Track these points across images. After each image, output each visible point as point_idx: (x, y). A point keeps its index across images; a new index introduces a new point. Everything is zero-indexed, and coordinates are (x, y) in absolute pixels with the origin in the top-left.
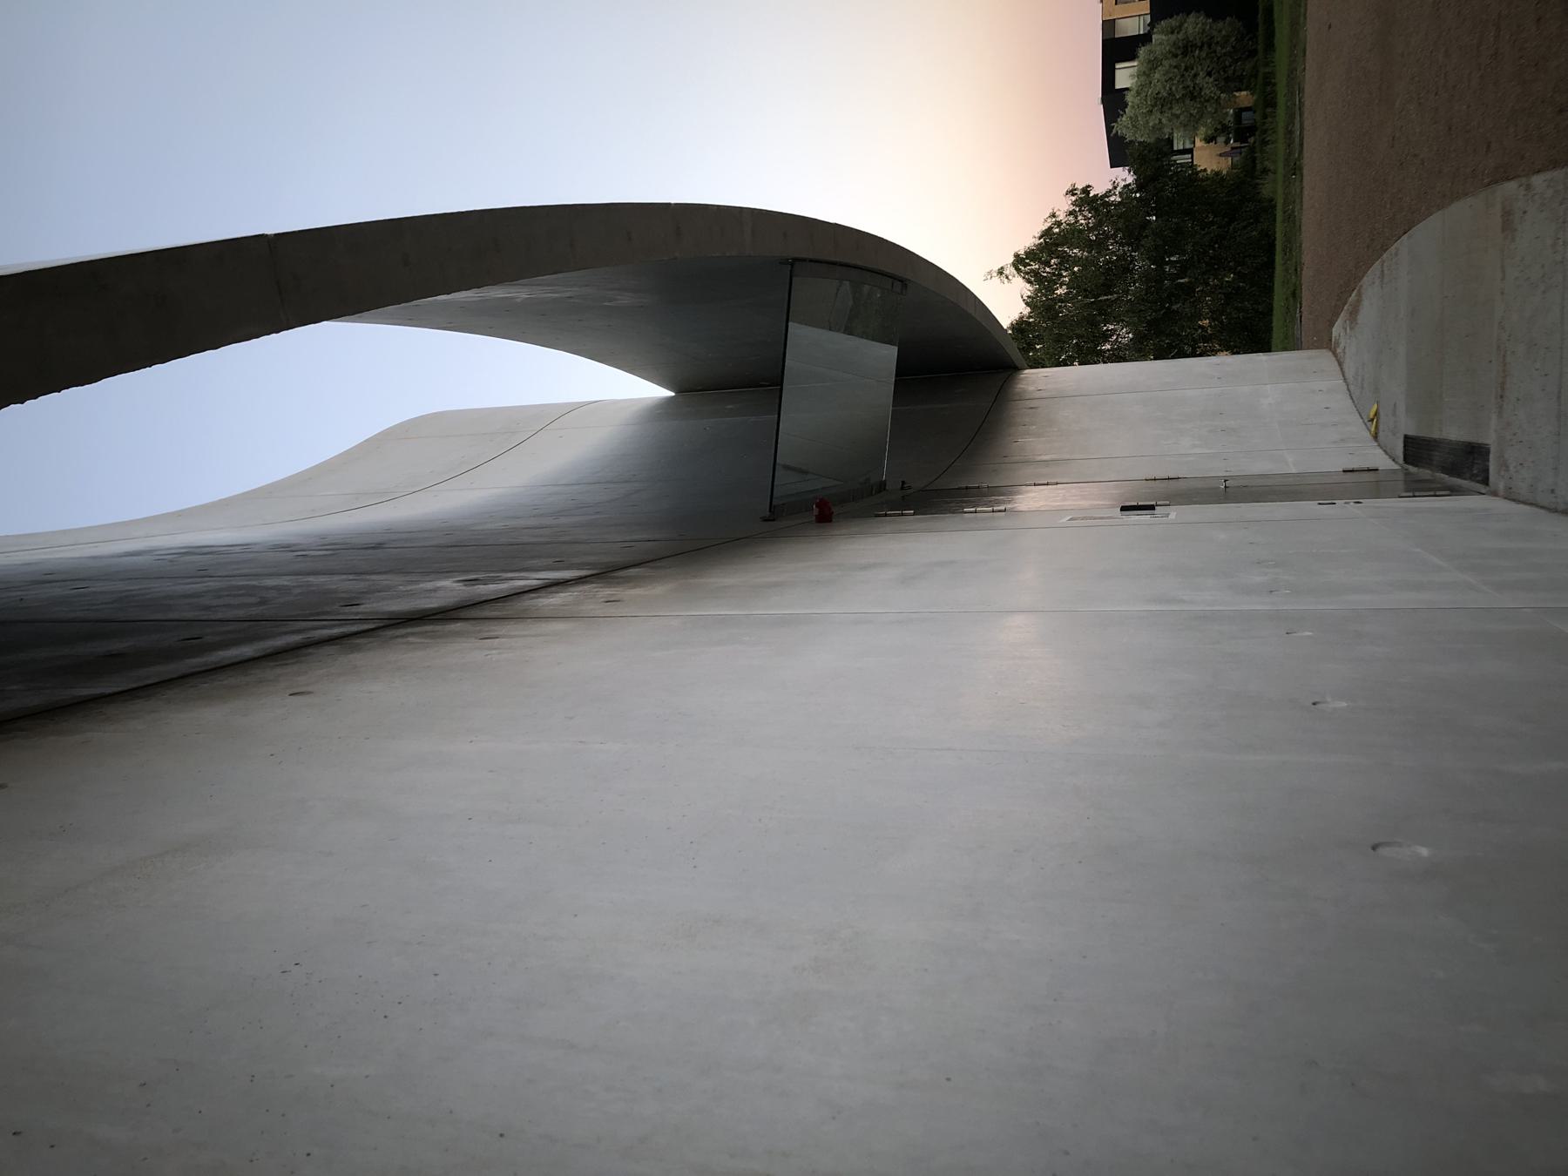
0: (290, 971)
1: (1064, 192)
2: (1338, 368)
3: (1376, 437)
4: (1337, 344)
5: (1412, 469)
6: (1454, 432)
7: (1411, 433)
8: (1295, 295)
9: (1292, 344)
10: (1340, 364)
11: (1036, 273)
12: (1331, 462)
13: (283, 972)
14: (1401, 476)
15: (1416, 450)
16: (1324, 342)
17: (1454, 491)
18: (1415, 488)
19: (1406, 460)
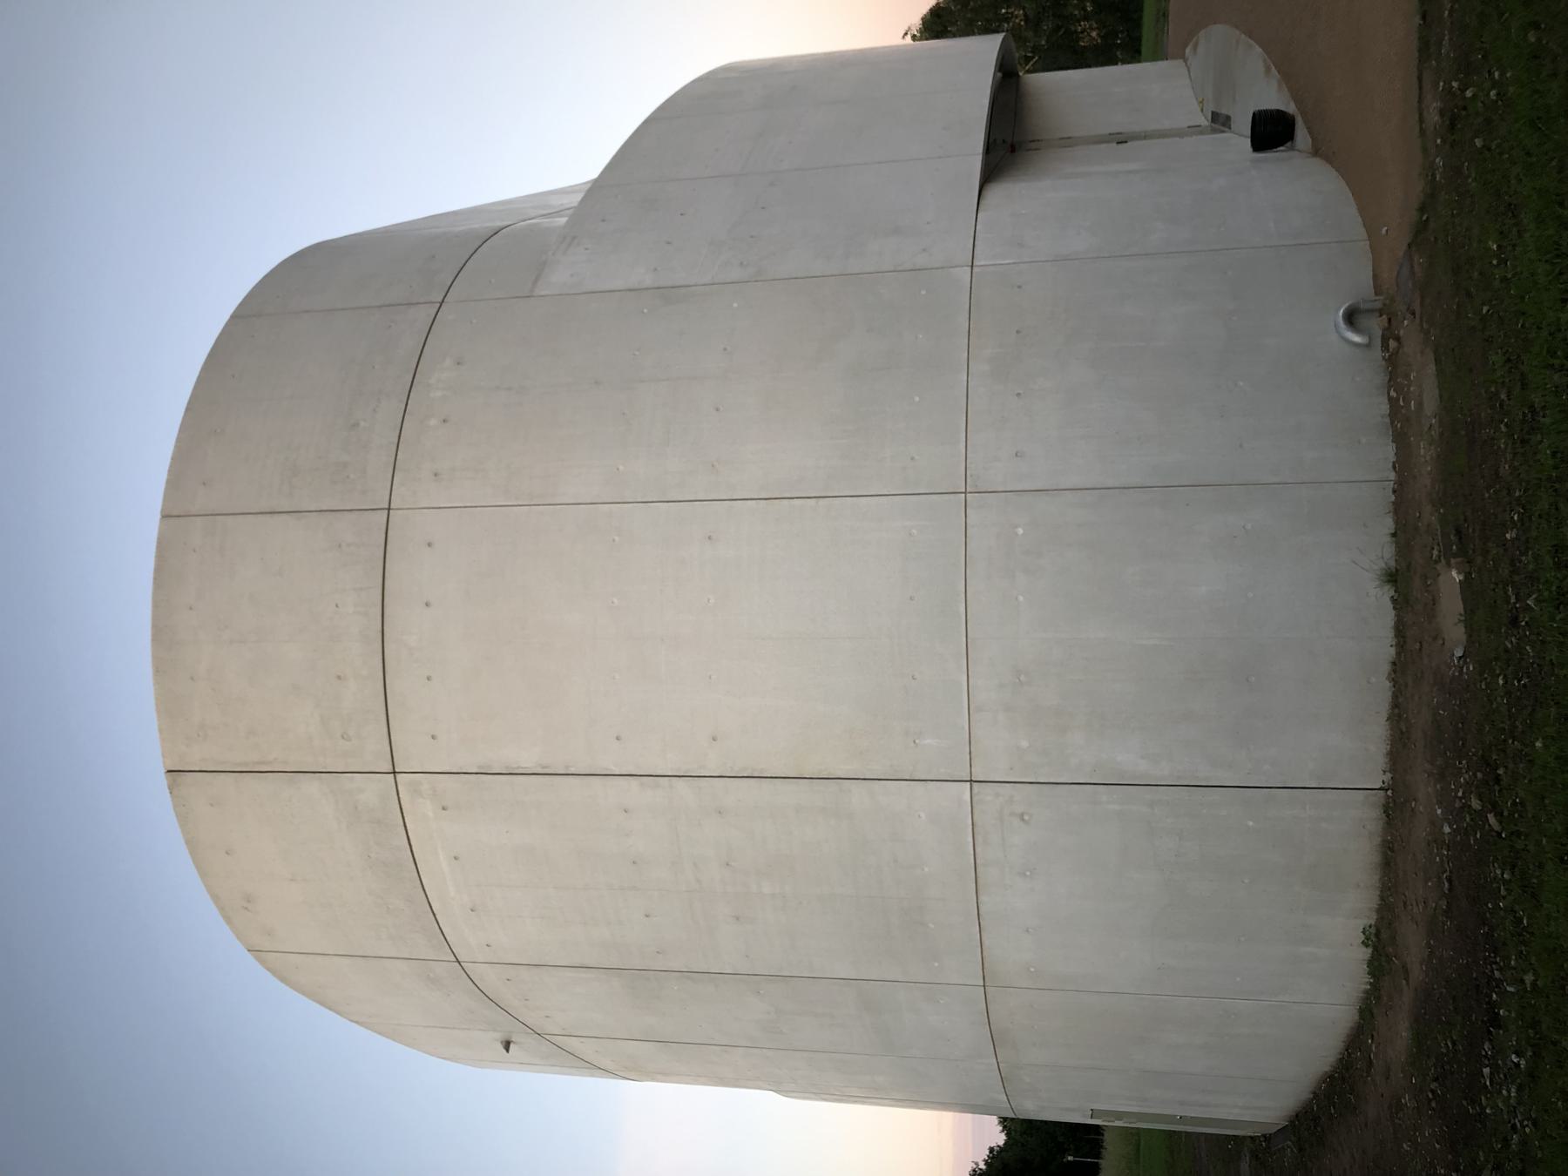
0: (1358, 548)
1: (504, 1051)
2: (1187, 72)
3: (1202, 110)
4: (1187, 59)
5: (1213, 125)
6: (1224, 111)
7: (1214, 110)
8: (1164, 15)
9: (1159, 55)
10: (1189, 71)
11: (1389, 803)
12: (1183, 122)
13: (1354, 562)
14: (1209, 128)
15: (1215, 117)
16: (1181, 56)
17: (1223, 132)
18: (1214, 131)
19: (1212, 121)
